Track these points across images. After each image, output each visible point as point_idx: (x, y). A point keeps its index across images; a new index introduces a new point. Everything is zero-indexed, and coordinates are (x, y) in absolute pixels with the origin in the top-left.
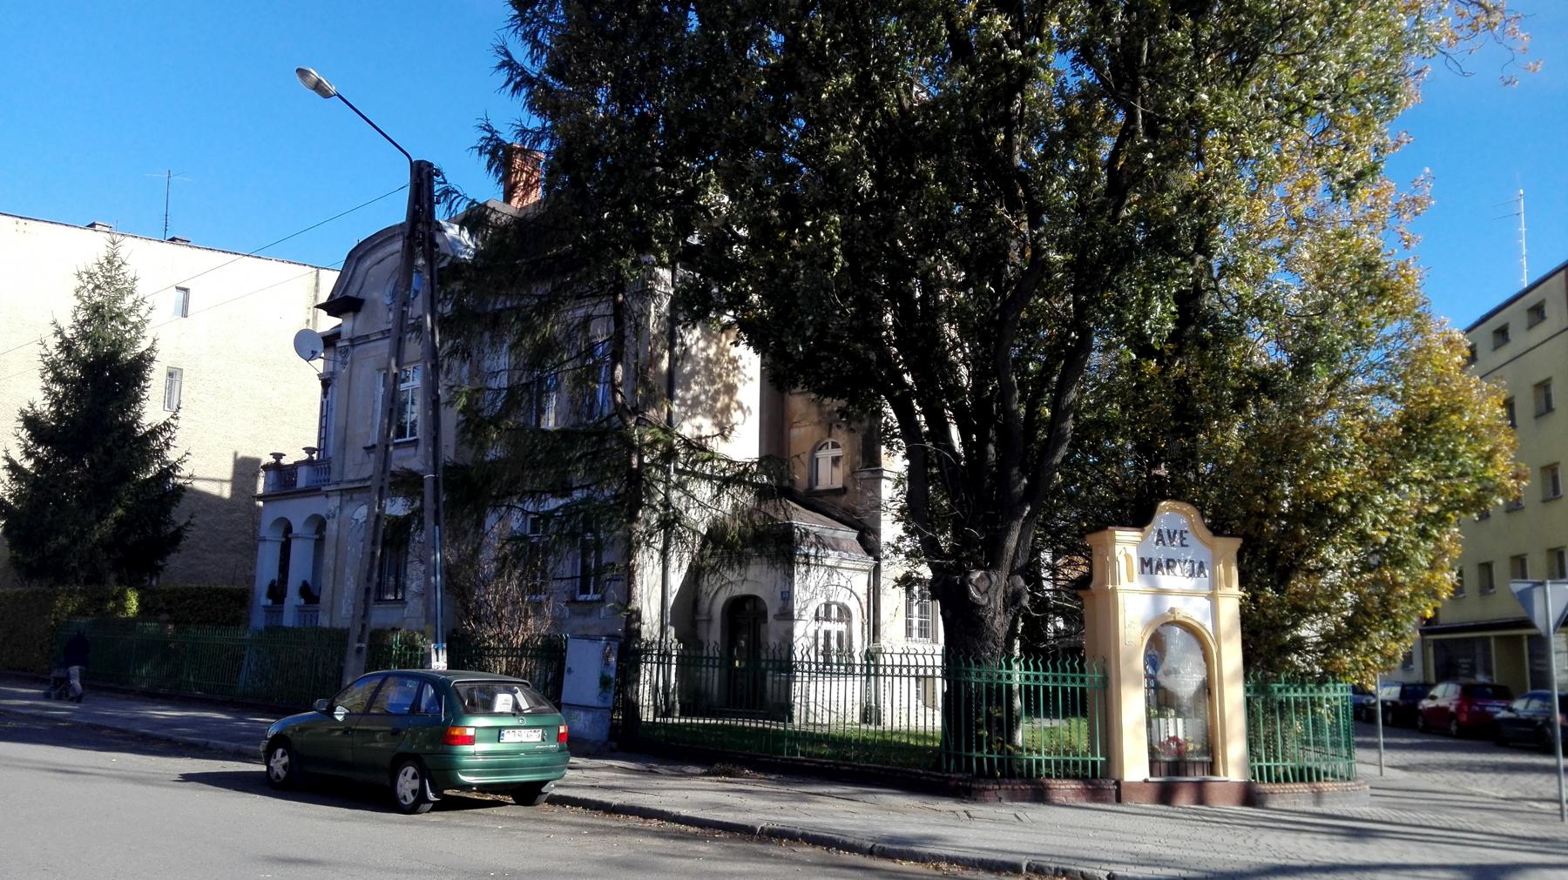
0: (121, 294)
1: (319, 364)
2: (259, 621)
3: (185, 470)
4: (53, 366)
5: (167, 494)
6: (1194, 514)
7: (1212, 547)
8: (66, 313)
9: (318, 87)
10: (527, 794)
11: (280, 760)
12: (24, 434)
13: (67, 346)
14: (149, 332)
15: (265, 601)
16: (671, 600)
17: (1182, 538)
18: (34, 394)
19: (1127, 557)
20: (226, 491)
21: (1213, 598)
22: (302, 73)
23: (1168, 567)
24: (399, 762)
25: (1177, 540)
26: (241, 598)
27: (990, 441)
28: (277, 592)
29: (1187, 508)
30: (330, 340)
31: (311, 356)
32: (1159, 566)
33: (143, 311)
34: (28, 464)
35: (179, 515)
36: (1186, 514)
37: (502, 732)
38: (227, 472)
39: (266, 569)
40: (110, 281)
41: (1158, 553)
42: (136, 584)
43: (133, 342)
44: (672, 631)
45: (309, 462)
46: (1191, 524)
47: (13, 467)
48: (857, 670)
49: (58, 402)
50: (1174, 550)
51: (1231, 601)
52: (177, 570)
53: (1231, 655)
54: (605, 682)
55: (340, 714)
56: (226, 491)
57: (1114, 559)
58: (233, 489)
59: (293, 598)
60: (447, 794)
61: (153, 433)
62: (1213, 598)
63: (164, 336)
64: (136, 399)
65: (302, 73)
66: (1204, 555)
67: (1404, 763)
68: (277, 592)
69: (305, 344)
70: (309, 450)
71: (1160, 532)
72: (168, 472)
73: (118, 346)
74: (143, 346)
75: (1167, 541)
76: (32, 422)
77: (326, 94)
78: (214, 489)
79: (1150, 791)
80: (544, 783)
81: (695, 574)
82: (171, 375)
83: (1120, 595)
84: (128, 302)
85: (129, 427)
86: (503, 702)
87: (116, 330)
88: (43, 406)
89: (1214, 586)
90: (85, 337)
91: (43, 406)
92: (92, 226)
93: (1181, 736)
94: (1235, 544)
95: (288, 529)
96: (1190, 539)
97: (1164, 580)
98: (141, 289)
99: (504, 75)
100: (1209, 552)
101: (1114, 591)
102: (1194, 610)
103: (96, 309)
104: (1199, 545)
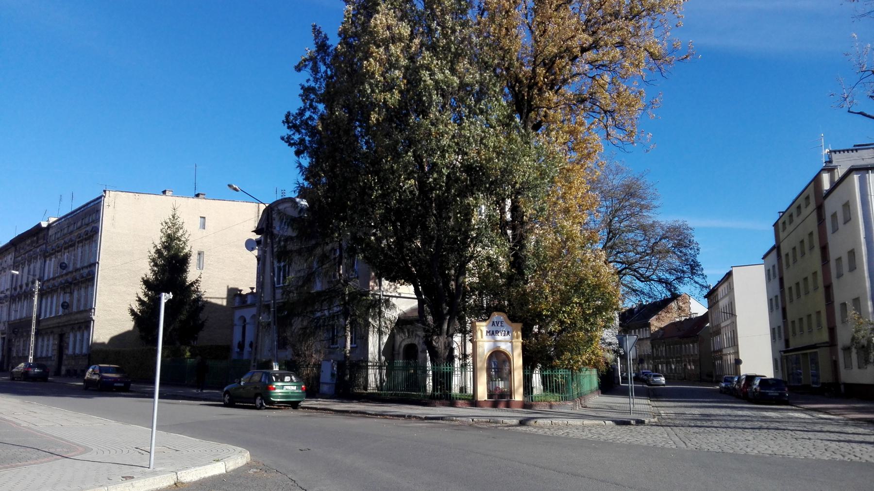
0: (178, 229)
1: (256, 252)
2: (234, 356)
3: (206, 295)
4: (153, 260)
5: (200, 306)
6: (505, 316)
8: (157, 239)
9: (235, 189)
10: (295, 405)
11: (227, 398)
12: (144, 287)
13: (158, 252)
14: (188, 244)
15: (237, 349)
16: (382, 348)
18: (146, 270)
20: (224, 303)
22: (230, 186)
24: (257, 395)
26: (228, 349)
28: (241, 346)
30: (258, 242)
31: (252, 249)
33: (186, 236)
34: (146, 299)
35: (202, 316)
37: (285, 387)
38: (224, 294)
39: (237, 338)
40: (174, 225)
41: (494, 328)
42: (188, 344)
43: (183, 248)
44: (383, 358)
45: (252, 293)
47: (140, 300)
49: (155, 274)
51: (519, 342)
52: (205, 338)
54: (333, 375)
55: (242, 383)
56: (224, 303)
58: (228, 302)
59: (247, 347)
60: (270, 404)
61: (192, 284)
63: (194, 241)
64: (185, 271)
65: (230, 186)
68: (241, 346)
69: (250, 245)
70: (252, 289)
72: (199, 298)
73: (180, 249)
74: (187, 250)
76: (146, 282)
77: (237, 190)
78: (219, 302)
79: (489, 404)
80: (300, 402)
81: (392, 337)
82: (199, 254)
84: (181, 232)
85: (185, 281)
86: (287, 379)
87: (176, 244)
88: (151, 276)
89: (512, 338)
90: (165, 247)
91: (151, 276)
92: (164, 192)
95: (245, 321)
96: (504, 324)
98: (185, 227)
99: (298, 170)
102: (505, 347)
103: (169, 236)
104: (507, 325)
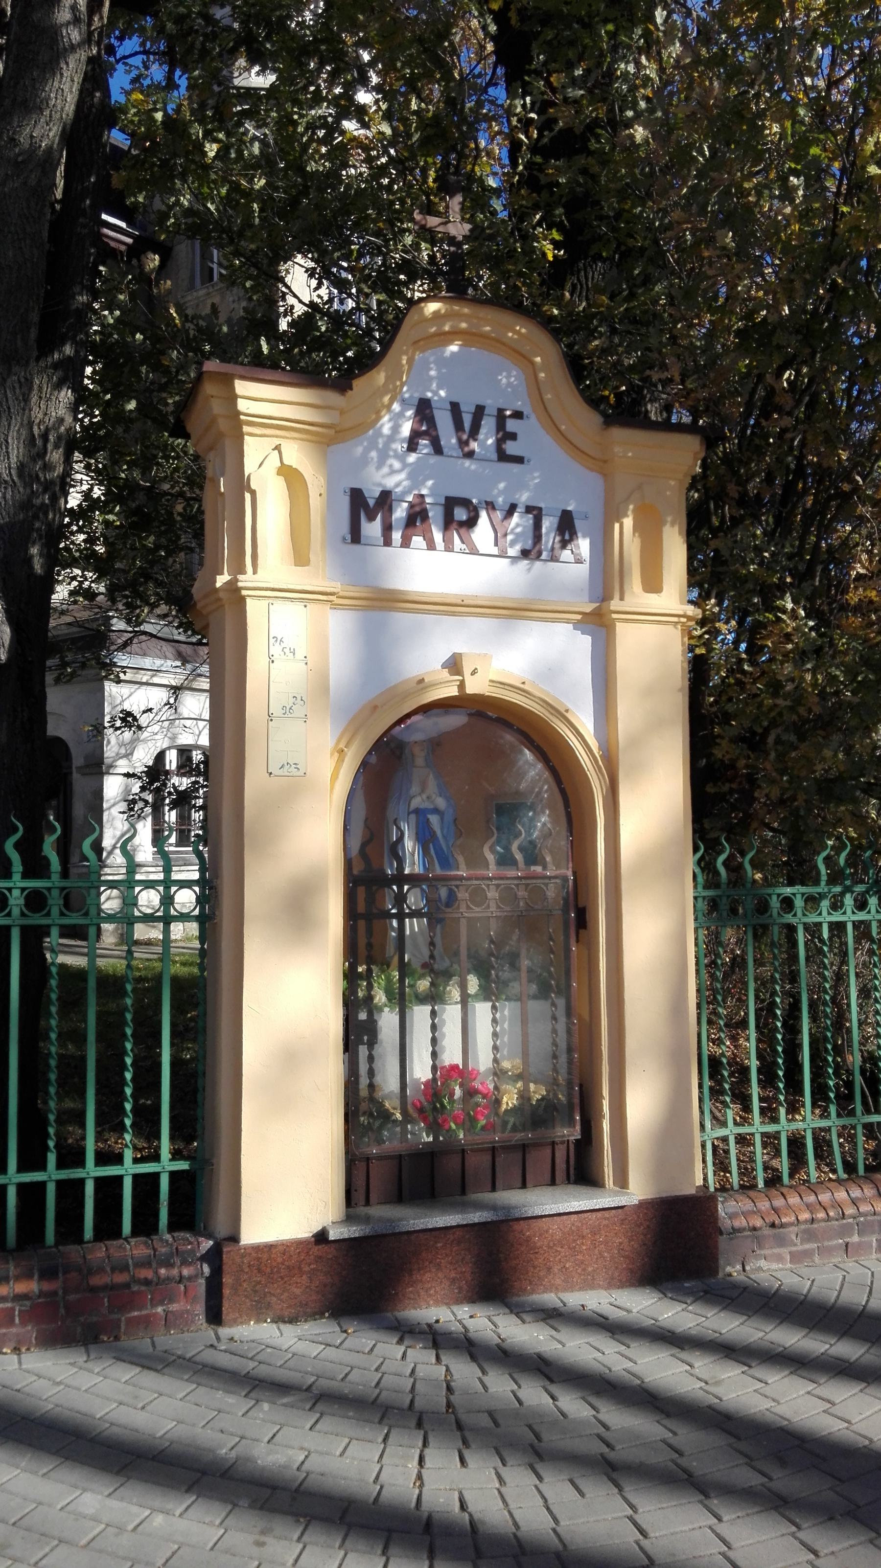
7: (601, 464)
17: (505, 436)
19: (287, 473)
21: (599, 623)
23: (448, 522)
25: (487, 439)
27: (805, 510)
29: (519, 330)
32: (417, 518)
36: (520, 356)
46: (536, 388)
48: (414, 899)
50: (472, 476)
51: (659, 621)
53: (650, 808)
57: (242, 484)
62: (599, 623)
66: (578, 491)
67: (362, 1380)
71: (424, 410)
75: (449, 439)
83: (254, 609)
93: (483, 1060)
94: (682, 456)
96: (531, 436)
97: (425, 567)
100: (594, 481)
101: (236, 598)
102: (528, 660)
